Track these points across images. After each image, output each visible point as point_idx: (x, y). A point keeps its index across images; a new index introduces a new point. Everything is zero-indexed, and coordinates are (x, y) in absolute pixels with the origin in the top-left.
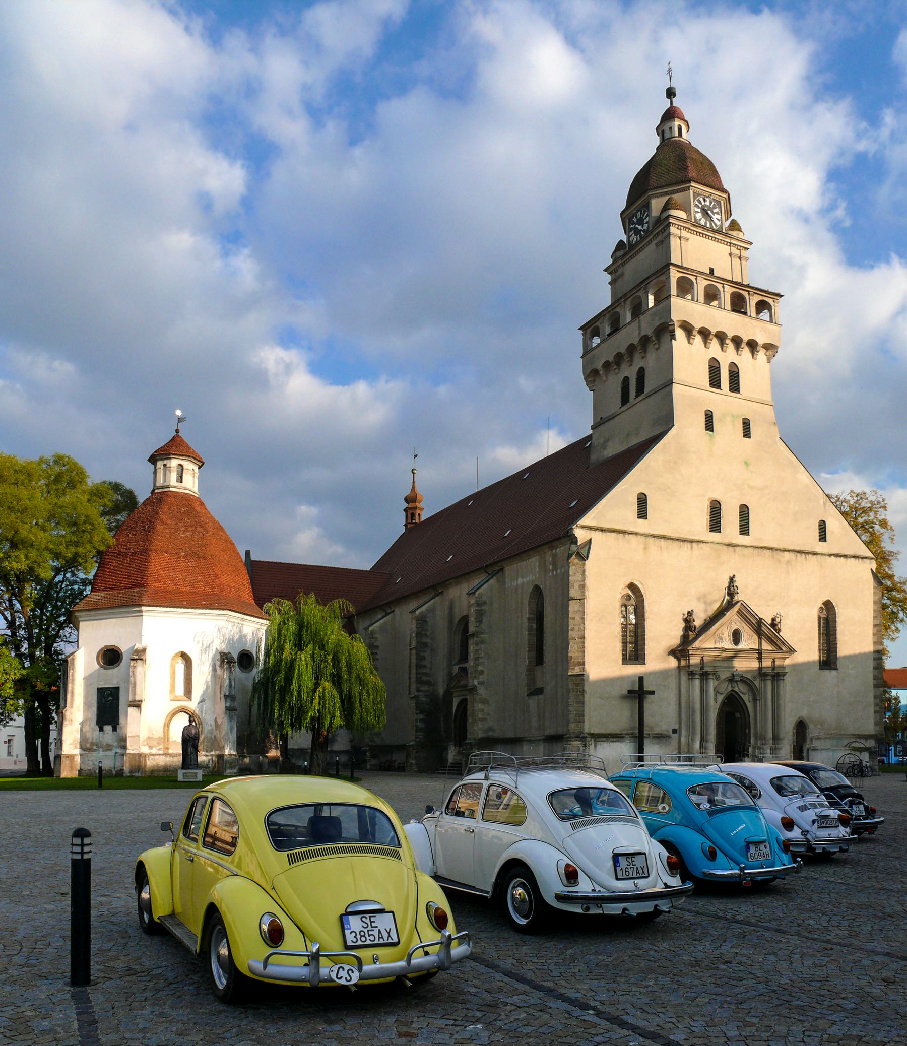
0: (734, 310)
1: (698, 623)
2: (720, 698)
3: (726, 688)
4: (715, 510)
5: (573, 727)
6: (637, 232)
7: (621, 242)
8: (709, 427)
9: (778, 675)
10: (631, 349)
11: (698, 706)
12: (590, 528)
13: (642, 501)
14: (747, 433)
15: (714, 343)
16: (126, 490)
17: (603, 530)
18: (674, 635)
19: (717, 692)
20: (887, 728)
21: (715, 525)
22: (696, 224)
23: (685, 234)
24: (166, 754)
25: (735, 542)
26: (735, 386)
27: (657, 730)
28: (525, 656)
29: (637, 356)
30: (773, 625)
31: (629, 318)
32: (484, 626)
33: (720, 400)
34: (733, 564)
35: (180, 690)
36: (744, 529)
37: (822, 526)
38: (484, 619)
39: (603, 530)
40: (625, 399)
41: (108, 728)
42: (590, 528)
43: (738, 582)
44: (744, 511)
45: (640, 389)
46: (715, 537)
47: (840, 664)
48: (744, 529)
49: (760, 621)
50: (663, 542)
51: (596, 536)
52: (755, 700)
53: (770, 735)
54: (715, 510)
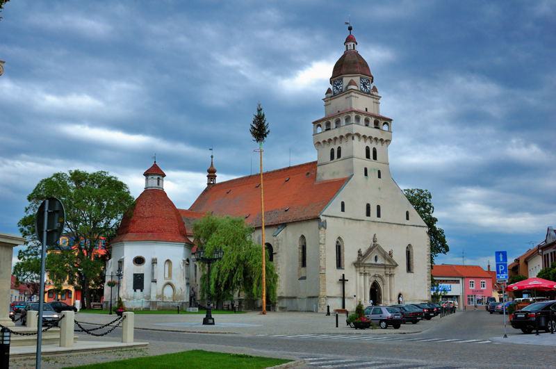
0: (375, 128)
1: (363, 252)
2: (371, 283)
3: (373, 279)
4: (368, 207)
5: (321, 293)
6: (337, 89)
7: (329, 89)
8: (366, 174)
9: (17, 311)
10: (336, 138)
11: (363, 286)
12: (325, 216)
13: (343, 204)
14: (379, 177)
15: (368, 141)
16: (91, 176)
17: (329, 216)
18: (355, 257)
19: (370, 281)
20: (432, 297)
21: (368, 214)
22: (361, 91)
23: (357, 95)
24: (163, 302)
25: (375, 220)
26: (375, 158)
27: (348, 296)
28: (298, 263)
29: (337, 142)
30: (390, 254)
31: (334, 126)
32: (280, 249)
33: (370, 164)
34: (375, 229)
35: (167, 276)
36: (379, 216)
37: (407, 214)
38: (280, 246)
39: (329, 216)
40: (332, 158)
41: (138, 291)
42: (325, 216)
43: (377, 237)
44: (379, 208)
45: (339, 156)
46: (368, 218)
47: (494, 254)
48: (379, 216)
49: (385, 252)
50: (350, 221)
51: (328, 220)
52: (383, 284)
53: (389, 299)
54: (368, 207)
